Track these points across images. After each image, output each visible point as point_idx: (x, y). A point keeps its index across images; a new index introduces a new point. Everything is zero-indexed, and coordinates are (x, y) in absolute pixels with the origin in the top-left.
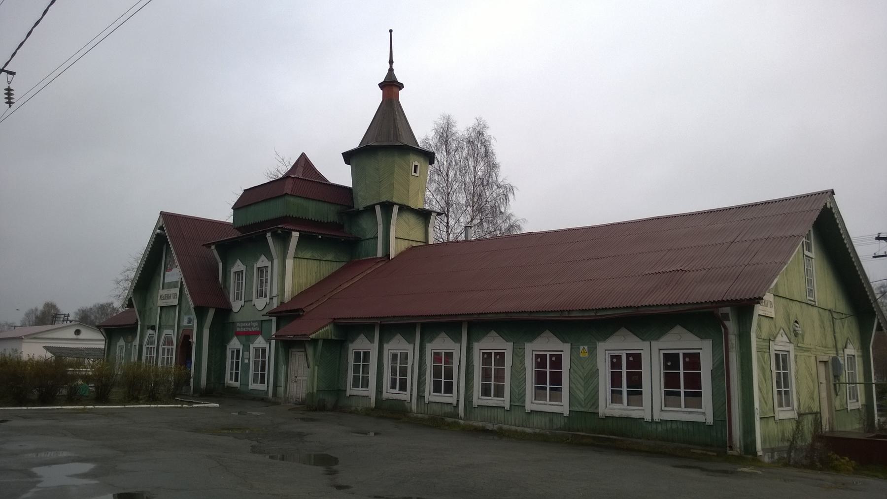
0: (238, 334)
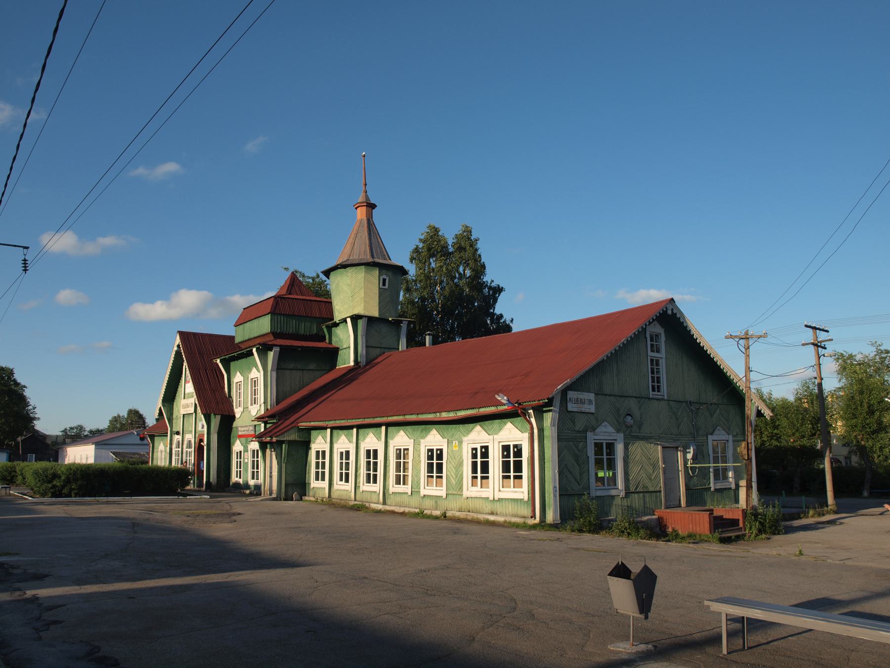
0: (240, 436)
